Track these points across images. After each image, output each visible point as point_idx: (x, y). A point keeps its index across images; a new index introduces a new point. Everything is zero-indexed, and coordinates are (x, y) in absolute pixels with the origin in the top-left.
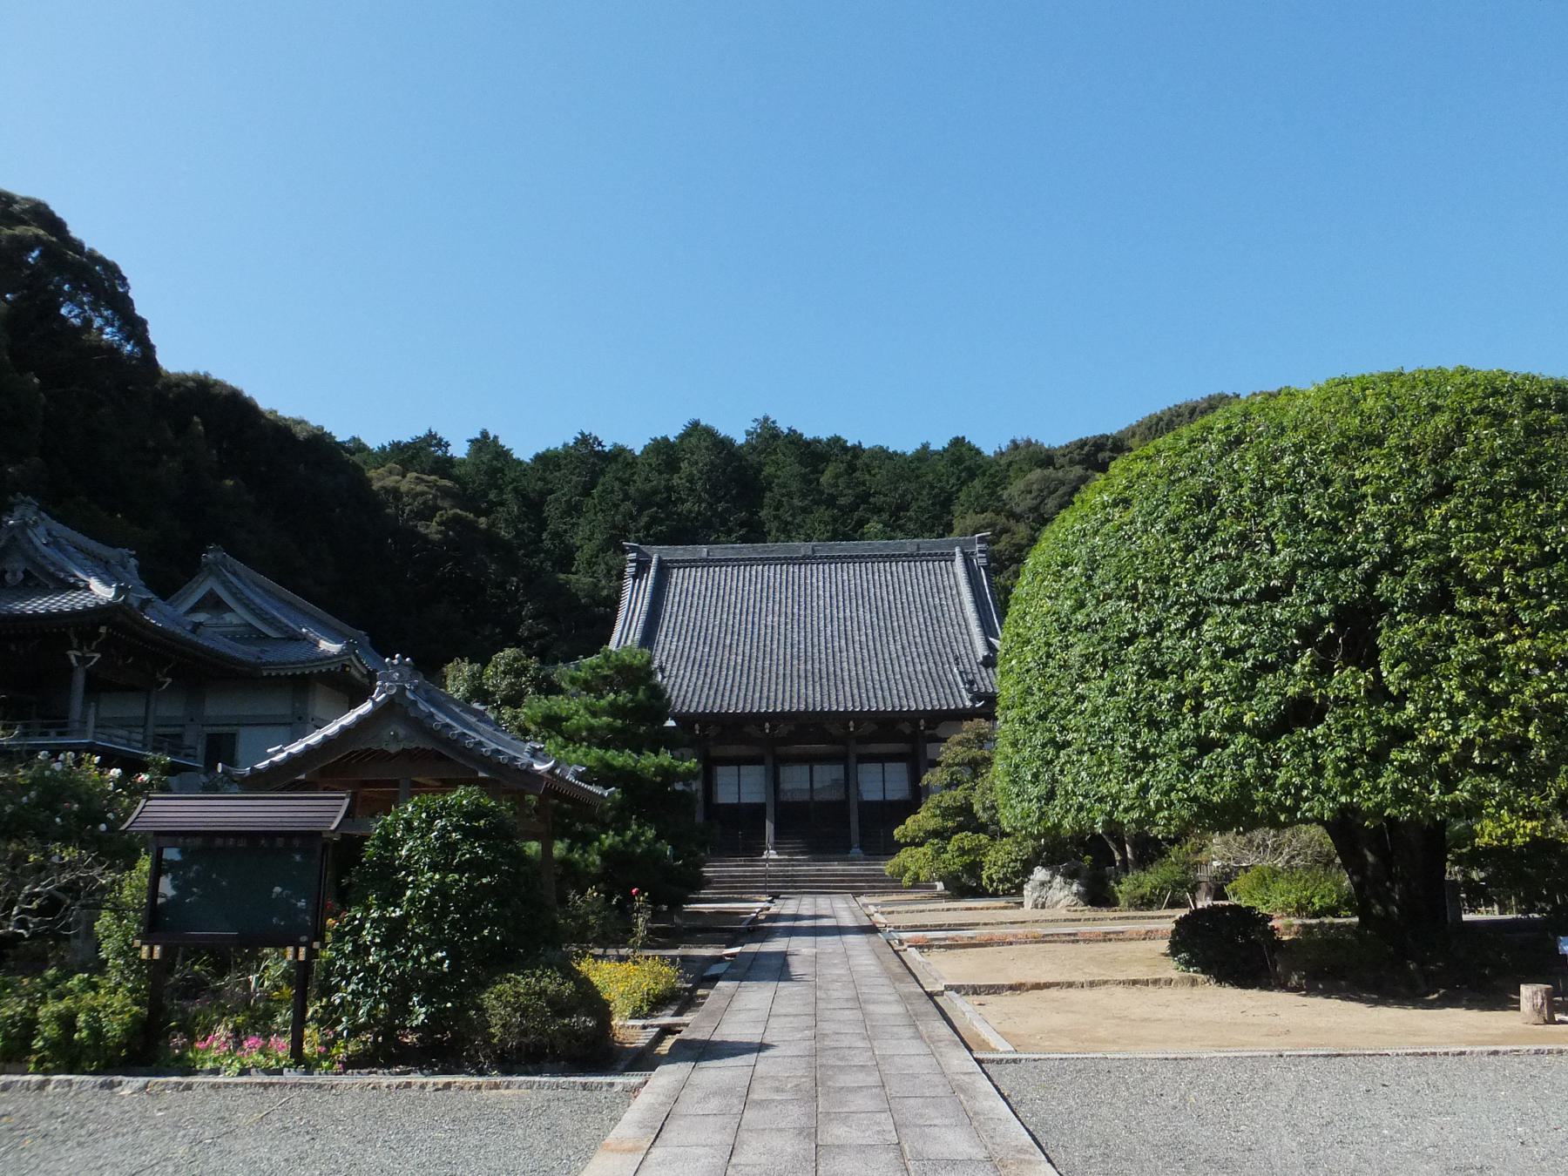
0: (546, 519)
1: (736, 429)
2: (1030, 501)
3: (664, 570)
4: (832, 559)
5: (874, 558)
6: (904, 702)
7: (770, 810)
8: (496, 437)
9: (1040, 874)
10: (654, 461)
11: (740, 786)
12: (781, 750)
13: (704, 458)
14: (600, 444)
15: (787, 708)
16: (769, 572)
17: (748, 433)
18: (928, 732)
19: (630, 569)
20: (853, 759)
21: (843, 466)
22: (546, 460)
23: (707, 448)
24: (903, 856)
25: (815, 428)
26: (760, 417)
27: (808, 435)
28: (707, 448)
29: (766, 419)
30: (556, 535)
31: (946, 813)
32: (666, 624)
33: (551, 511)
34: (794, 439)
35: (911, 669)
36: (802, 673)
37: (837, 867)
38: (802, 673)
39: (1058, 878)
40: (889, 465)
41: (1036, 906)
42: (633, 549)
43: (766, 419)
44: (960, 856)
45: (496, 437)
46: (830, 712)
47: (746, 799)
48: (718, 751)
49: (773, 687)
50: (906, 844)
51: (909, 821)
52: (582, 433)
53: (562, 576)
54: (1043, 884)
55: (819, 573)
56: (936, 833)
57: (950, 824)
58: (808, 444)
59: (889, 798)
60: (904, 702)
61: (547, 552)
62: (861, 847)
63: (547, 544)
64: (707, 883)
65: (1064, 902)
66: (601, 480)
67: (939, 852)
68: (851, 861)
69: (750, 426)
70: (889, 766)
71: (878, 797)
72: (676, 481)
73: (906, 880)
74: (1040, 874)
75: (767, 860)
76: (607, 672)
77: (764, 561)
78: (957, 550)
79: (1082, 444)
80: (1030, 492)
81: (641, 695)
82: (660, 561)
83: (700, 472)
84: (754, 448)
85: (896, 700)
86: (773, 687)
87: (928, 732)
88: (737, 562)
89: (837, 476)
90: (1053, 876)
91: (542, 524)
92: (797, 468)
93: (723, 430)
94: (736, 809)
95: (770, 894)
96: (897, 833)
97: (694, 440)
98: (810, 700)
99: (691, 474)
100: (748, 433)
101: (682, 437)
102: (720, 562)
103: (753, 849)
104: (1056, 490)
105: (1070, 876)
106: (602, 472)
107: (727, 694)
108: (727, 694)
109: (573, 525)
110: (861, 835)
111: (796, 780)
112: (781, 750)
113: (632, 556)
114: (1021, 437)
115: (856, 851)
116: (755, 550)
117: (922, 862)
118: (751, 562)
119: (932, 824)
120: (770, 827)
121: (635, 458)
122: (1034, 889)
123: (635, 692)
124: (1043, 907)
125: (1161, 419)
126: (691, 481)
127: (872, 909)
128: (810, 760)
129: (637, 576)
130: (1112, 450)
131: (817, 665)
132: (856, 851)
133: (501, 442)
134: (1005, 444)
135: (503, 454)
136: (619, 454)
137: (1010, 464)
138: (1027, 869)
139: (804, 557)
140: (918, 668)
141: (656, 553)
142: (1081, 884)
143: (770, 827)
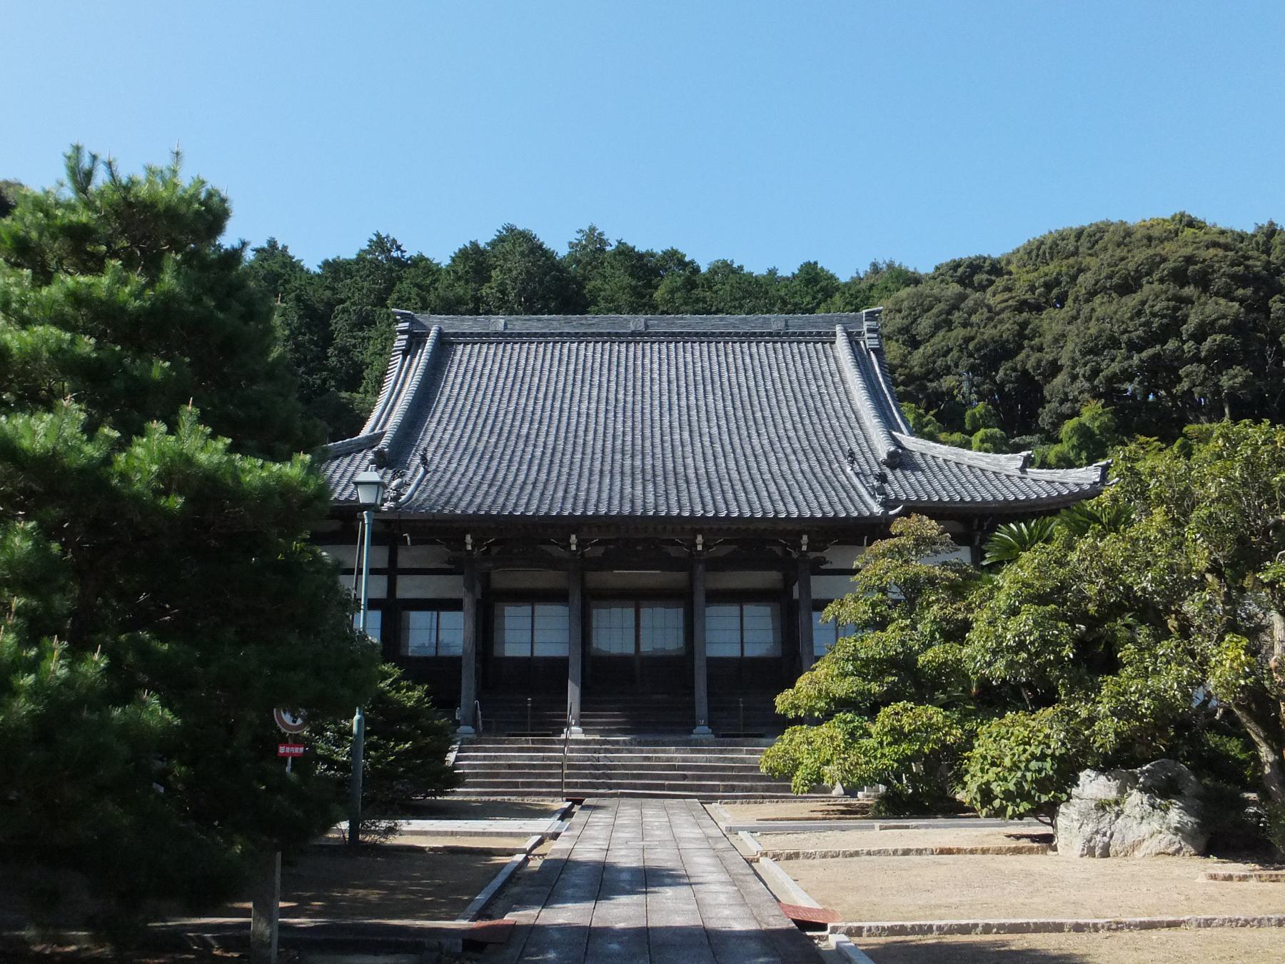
0: (332, 332)
1: (559, 241)
2: (898, 321)
3: (445, 345)
4: (673, 337)
5: (725, 337)
6: (780, 507)
7: (575, 670)
8: (285, 248)
9: (1093, 786)
10: (460, 269)
11: (536, 633)
12: (599, 579)
13: (518, 265)
14: (398, 248)
15: (603, 511)
16: (587, 351)
17: (571, 245)
18: (812, 555)
19: (400, 342)
20: (699, 598)
21: (679, 281)
22: (335, 268)
23: (522, 254)
24: (792, 740)
25: (648, 242)
26: (586, 228)
27: (641, 248)
28: (522, 254)
29: (592, 229)
30: (344, 351)
31: (871, 668)
32: (441, 406)
33: (339, 324)
34: (625, 252)
35: (785, 467)
36: (628, 470)
37: (674, 755)
38: (628, 470)
39: (1136, 800)
40: (733, 279)
41: (1091, 852)
42: (405, 318)
43: (592, 229)
44: (896, 742)
45: (285, 248)
46: (668, 517)
47: (541, 651)
48: (501, 580)
49: (584, 486)
50: (798, 721)
51: (802, 682)
52: (378, 235)
53: (344, 394)
54: (1102, 806)
55: (653, 353)
56: (845, 704)
57: (875, 688)
58: (641, 256)
59: (748, 653)
60: (780, 507)
61: (332, 370)
62: (581, 724)
63: (333, 361)
64: (452, 779)
65: (1152, 845)
66: (398, 286)
67: (853, 737)
68: (695, 745)
69: (575, 237)
70: (749, 609)
71: (732, 651)
72: (485, 291)
73: (797, 780)
74: (1093, 786)
75: (566, 742)
76: (84, 217)
77: (580, 337)
78: (838, 328)
79: (956, 265)
80: (900, 311)
81: (169, 280)
82: (441, 334)
83: (514, 280)
84: (578, 262)
85: (768, 505)
86: (584, 486)
87: (812, 555)
88: (543, 337)
89: (672, 292)
90: (1122, 791)
91: (328, 339)
92: (627, 280)
93: (549, 244)
94: (528, 664)
95: (569, 797)
96: (783, 702)
97: (508, 246)
98: (639, 502)
99: (502, 284)
100: (571, 245)
101: (493, 244)
102: (520, 338)
103: (547, 724)
104: (928, 310)
105: (1163, 790)
106: (400, 279)
107: (516, 492)
108: (516, 492)
109: (363, 339)
110: (710, 709)
111: (615, 633)
112: (599, 579)
113: (404, 326)
114: (882, 260)
115: (702, 731)
116: (569, 322)
117: (827, 753)
118: (563, 337)
119: (842, 688)
120: (573, 693)
121: (439, 270)
122: (1084, 815)
123: (153, 267)
124: (1106, 853)
125: (1042, 243)
126: (503, 292)
127: (751, 845)
128: (637, 597)
129: (409, 351)
130: (989, 273)
131: (649, 460)
132: (702, 731)
133: (291, 252)
134: (864, 268)
135: (292, 266)
136: (420, 263)
137: (871, 287)
138: (1064, 775)
139: (633, 334)
140: (796, 467)
141: (435, 324)
142: (1187, 810)
143: (573, 693)
